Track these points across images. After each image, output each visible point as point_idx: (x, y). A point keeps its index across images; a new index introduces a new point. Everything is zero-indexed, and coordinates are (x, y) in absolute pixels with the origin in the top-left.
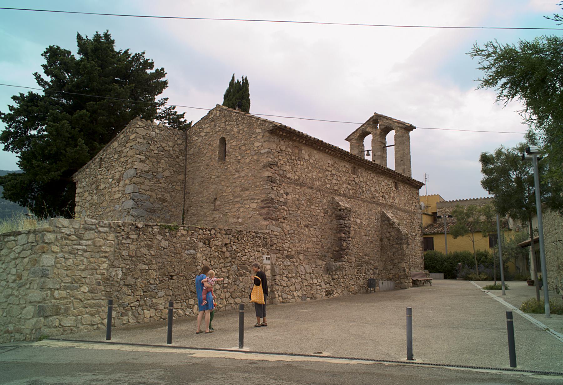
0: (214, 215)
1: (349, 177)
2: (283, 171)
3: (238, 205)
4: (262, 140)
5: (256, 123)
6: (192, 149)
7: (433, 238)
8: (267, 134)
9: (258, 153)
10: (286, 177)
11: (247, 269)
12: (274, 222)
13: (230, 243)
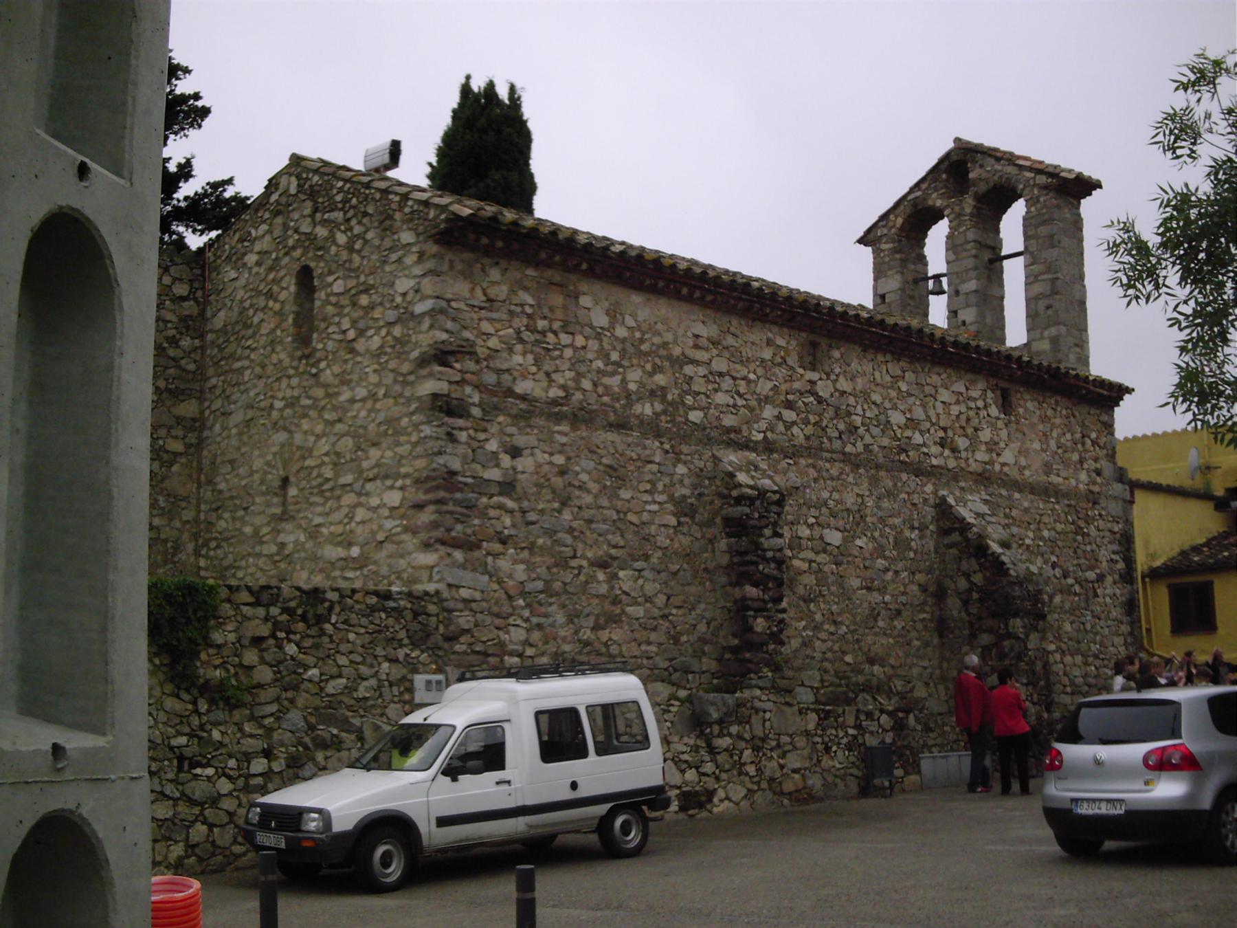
0: (282, 538)
1: (790, 379)
2: (498, 372)
3: (349, 499)
4: (418, 271)
5: (401, 209)
6: (222, 314)
7: (1212, 582)
8: (432, 248)
9: (407, 317)
10: (510, 392)
11: (345, 725)
12: (458, 555)
13: (273, 636)
